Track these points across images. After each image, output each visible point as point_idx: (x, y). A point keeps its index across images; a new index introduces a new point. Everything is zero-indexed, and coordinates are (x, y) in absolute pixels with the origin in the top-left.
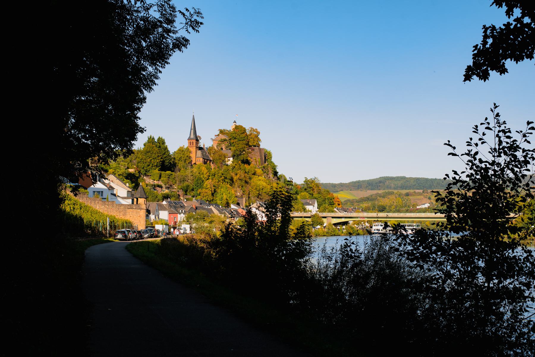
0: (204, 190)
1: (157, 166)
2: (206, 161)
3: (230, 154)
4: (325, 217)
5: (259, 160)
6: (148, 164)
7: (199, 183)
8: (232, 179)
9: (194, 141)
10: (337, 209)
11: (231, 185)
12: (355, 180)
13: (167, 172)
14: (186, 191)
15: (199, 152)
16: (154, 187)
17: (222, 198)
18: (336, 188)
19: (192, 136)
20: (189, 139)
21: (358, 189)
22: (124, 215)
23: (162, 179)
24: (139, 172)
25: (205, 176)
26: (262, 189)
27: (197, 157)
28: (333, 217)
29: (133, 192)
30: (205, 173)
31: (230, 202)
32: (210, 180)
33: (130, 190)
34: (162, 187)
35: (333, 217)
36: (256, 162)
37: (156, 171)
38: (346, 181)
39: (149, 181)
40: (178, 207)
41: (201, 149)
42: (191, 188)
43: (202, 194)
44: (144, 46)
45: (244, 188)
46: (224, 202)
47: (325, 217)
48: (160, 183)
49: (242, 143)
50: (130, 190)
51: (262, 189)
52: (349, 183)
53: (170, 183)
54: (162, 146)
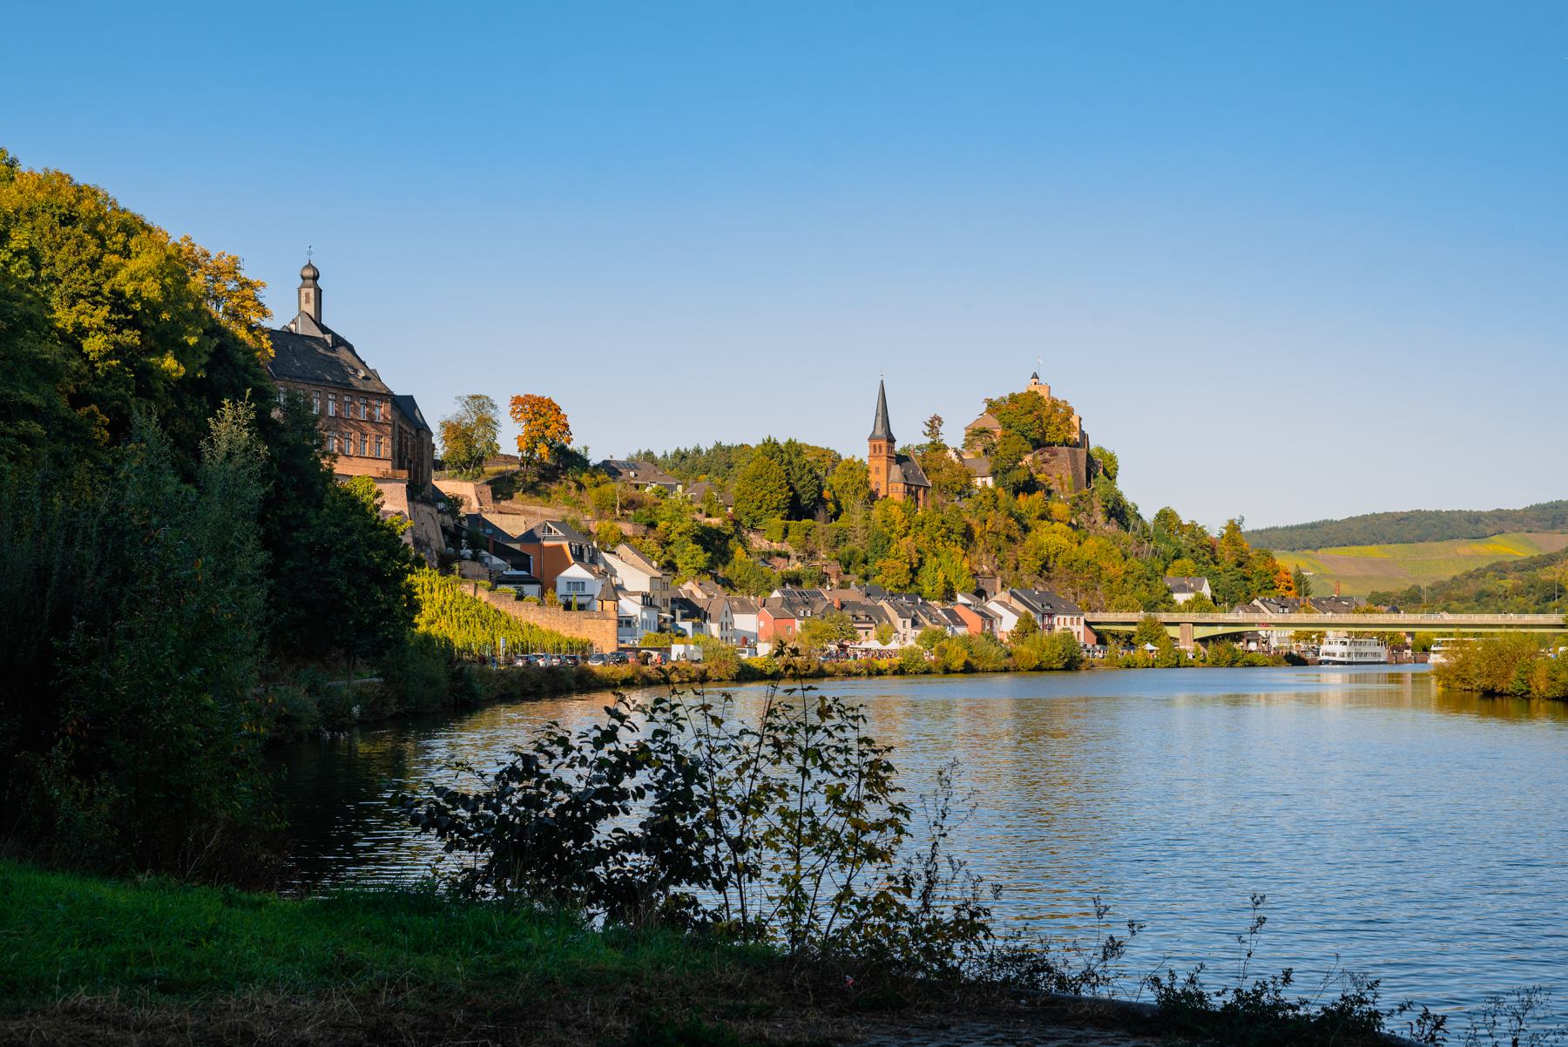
0: (889, 562)
1: (778, 508)
2: (912, 491)
3: (987, 469)
4: (1177, 624)
5: (1068, 477)
6: (757, 503)
7: (882, 544)
8: (968, 534)
9: (884, 443)
10: (1262, 602)
11: (965, 547)
12: (1545, 498)
13: (804, 521)
14: (848, 565)
15: (896, 470)
16: (768, 556)
17: (935, 579)
18: (1481, 526)
19: (879, 432)
20: (872, 438)
21: (1554, 526)
22: (579, 629)
23: (790, 537)
24: (737, 523)
25: (898, 528)
26: (1056, 555)
27: (888, 482)
28: (1195, 624)
29: (666, 579)
30: (898, 519)
31: (957, 588)
32: (909, 538)
33: (659, 575)
34: (788, 557)
35: (1195, 624)
36: (1062, 485)
37: (777, 521)
38: (1517, 501)
39: (759, 542)
40: (797, 605)
41: (901, 459)
42: (862, 557)
43: (885, 571)
44: (137, 341)
45: (1005, 553)
46: (940, 588)
47: (1177, 624)
48: (786, 547)
49: (1032, 432)
50: (659, 575)
51: (1056, 555)
52: (1526, 510)
53: (810, 546)
54: (794, 460)
